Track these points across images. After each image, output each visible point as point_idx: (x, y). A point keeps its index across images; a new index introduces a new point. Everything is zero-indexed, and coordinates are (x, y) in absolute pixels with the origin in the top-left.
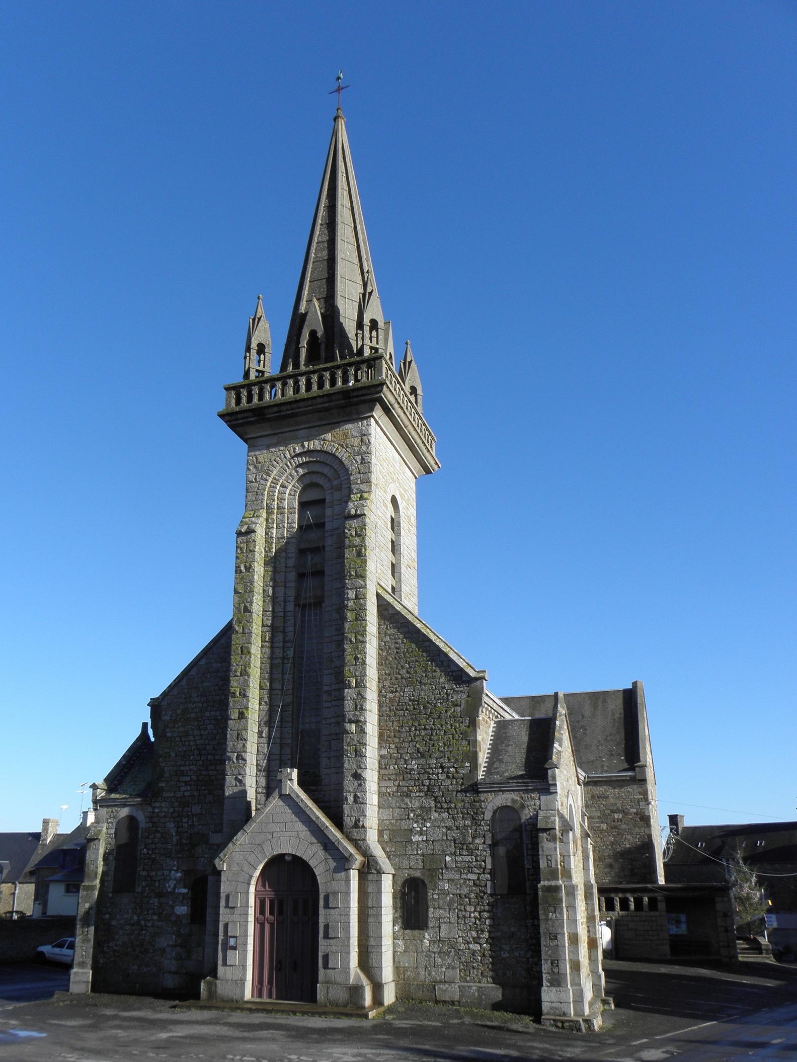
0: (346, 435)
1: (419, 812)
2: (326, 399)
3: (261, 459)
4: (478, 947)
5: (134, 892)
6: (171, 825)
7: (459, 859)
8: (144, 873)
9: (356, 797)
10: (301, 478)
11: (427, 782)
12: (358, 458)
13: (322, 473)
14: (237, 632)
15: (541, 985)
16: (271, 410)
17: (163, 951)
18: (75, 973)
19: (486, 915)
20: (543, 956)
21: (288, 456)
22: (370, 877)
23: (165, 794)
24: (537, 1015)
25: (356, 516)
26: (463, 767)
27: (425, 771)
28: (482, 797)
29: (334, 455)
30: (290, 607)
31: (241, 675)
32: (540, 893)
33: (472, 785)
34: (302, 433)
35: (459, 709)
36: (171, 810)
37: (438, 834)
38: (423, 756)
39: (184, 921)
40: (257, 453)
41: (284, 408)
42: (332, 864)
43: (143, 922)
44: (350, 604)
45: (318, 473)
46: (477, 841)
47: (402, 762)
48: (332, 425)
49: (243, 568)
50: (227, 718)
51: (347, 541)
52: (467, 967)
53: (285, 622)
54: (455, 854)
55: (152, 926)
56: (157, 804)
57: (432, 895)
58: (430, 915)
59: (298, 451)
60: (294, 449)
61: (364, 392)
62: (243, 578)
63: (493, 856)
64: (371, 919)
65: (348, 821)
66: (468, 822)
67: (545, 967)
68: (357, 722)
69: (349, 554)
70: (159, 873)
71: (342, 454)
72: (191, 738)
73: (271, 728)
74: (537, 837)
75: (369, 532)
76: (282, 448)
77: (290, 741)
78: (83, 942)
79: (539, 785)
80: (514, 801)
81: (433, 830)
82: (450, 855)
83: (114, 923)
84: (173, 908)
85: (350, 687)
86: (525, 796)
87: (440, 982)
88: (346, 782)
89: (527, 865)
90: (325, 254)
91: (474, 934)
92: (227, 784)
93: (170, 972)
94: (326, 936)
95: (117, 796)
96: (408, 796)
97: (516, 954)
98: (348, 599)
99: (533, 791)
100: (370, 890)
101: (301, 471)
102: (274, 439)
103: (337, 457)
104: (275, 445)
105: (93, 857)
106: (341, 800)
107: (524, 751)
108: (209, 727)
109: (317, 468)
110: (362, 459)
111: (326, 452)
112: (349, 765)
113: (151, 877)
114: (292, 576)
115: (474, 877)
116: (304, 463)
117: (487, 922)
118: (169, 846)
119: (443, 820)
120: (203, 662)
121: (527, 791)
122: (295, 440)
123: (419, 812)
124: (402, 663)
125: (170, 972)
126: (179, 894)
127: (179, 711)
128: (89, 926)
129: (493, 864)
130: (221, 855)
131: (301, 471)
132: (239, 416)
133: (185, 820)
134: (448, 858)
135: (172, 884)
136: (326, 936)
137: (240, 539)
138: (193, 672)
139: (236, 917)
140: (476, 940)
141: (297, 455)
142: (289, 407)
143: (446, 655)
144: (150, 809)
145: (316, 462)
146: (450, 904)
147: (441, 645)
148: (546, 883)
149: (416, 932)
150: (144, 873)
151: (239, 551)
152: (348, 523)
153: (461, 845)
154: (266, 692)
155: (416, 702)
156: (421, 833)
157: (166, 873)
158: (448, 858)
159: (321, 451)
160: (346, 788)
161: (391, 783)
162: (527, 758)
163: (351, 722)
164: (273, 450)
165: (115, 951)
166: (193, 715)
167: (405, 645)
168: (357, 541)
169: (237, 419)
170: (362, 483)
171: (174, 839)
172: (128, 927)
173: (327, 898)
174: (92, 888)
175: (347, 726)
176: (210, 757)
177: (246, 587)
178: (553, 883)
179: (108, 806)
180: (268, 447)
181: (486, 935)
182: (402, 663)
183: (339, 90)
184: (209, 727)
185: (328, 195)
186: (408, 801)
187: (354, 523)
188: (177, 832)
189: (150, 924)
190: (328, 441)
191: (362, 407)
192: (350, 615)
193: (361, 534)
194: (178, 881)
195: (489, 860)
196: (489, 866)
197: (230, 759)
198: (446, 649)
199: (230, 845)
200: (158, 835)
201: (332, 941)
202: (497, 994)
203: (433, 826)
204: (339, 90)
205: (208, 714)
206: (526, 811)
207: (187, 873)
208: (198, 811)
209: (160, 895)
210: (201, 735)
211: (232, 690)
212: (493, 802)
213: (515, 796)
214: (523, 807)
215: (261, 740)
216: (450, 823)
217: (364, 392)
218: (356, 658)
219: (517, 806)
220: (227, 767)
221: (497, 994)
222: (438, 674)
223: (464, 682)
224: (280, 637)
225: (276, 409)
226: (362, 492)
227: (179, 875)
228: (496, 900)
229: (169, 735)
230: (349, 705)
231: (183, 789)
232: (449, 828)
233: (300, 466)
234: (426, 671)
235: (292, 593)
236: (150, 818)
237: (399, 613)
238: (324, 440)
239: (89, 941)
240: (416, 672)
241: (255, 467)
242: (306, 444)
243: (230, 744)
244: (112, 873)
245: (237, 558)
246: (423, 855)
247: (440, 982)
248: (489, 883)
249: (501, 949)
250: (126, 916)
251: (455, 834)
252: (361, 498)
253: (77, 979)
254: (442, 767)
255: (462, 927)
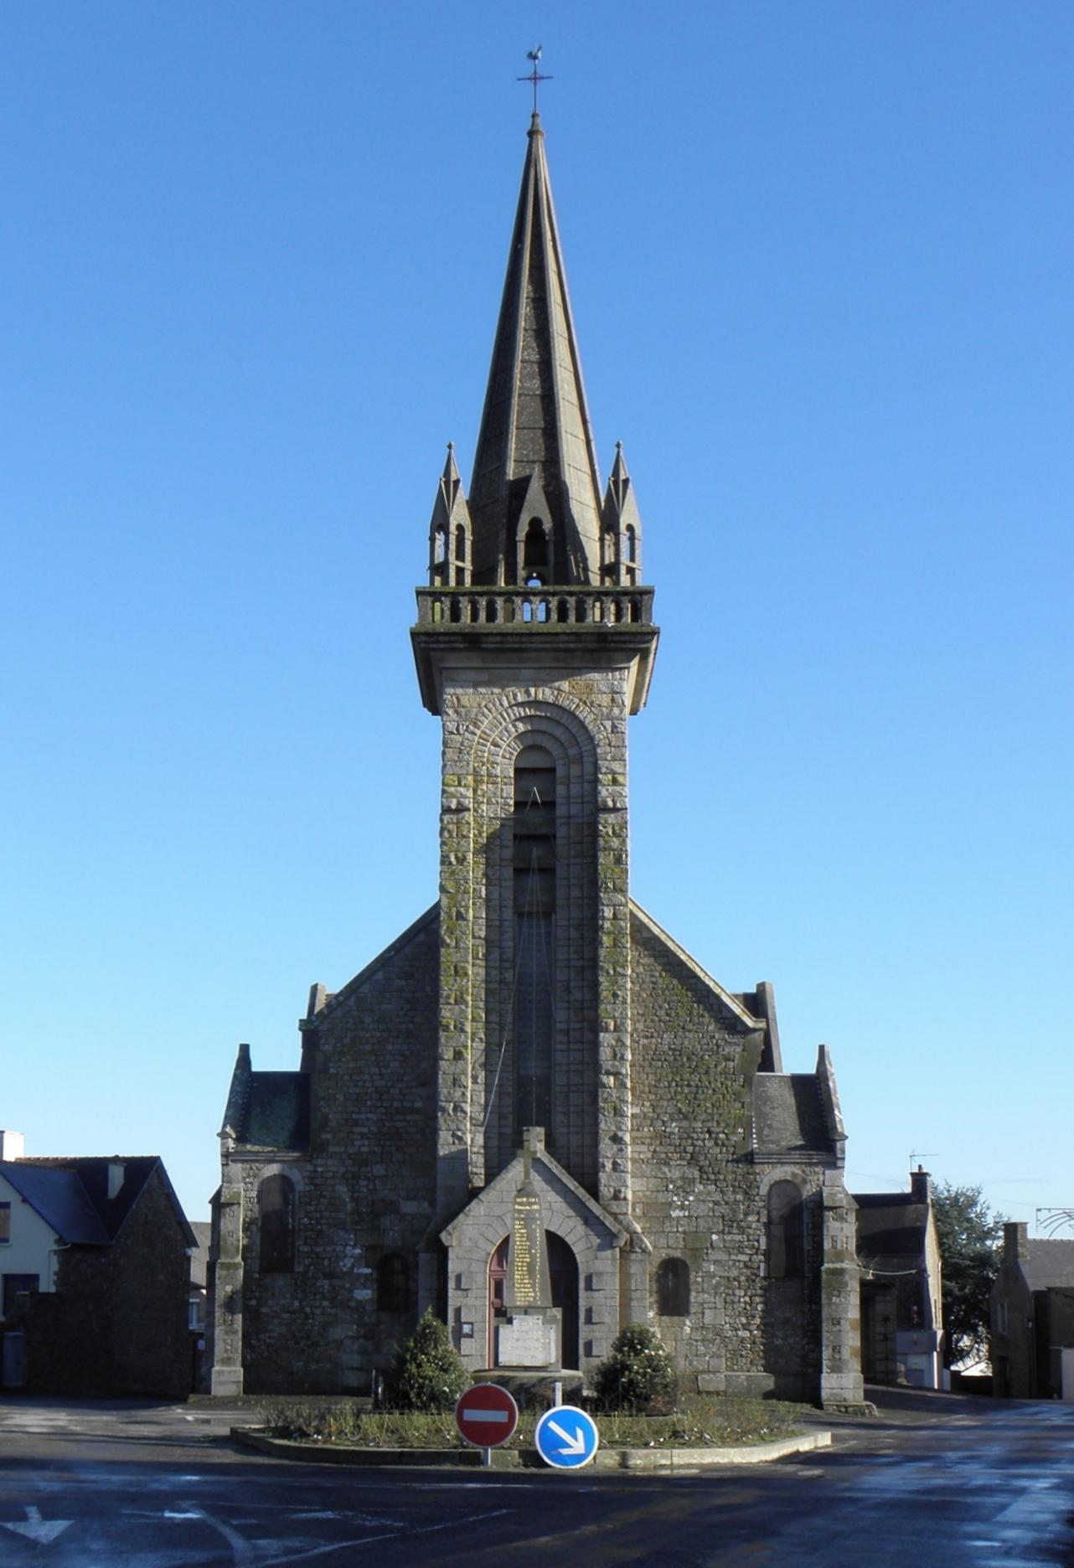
0: (590, 688)
1: (679, 1183)
2: (572, 638)
3: (465, 701)
4: (748, 1334)
5: (292, 1271)
6: (343, 1190)
7: (729, 1238)
8: (306, 1249)
9: (615, 1164)
10: (520, 737)
11: (690, 1149)
12: (608, 724)
13: (551, 735)
14: (448, 946)
15: (820, 1372)
16: (491, 639)
17: (339, 1344)
18: (219, 1372)
19: (758, 1299)
20: (825, 1342)
21: (506, 704)
22: (633, 1256)
23: (332, 1149)
24: (818, 1404)
25: (615, 810)
26: (734, 1133)
27: (687, 1135)
28: (758, 1169)
29: (572, 714)
30: (508, 914)
31: (456, 1003)
32: (824, 1276)
33: (746, 1155)
34: (526, 674)
35: (731, 1064)
36: (342, 1169)
37: (703, 1209)
38: (686, 1118)
39: (368, 1308)
40: (459, 691)
41: (510, 639)
42: (596, 1241)
43: (308, 1310)
44: (607, 925)
45: (545, 733)
46: (750, 1218)
47: (660, 1123)
48: (571, 671)
49: (453, 859)
50: (436, 1058)
51: (601, 842)
52: (735, 1355)
53: (501, 934)
54: (723, 1232)
55: (323, 1314)
56: (320, 1162)
57: (695, 1278)
58: (692, 1300)
59: (520, 699)
60: (515, 696)
61: (627, 638)
62: (453, 873)
63: (768, 1235)
64: (634, 1303)
65: (606, 1191)
66: (739, 1197)
67: (826, 1353)
68: (616, 1074)
69: (605, 860)
70: (328, 1249)
71: (584, 714)
72: (367, 1077)
73: (489, 1073)
74: (821, 1216)
75: (630, 831)
76: (497, 691)
77: (510, 1090)
78: (227, 1333)
79: (824, 1156)
80: (794, 1175)
81: (696, 1204)
82: (717, 1233)
83: (264, 1310)
84: (351, 1292)
85: (607, 1030)
86: (807, 1169)
87: (703, 1372)
88: (602, 1146)
89: (807, 1247)
90: (535, 384)
91: (744, 1320)
92: (441, 1141)
93: (352, 1369)
94: (589, 1321)
95: (256, 1148)
96: (666, 1164)
97: (791, 1341)
98: (604, 918)
99: (816, 1164)
100: (633, 1270)
101: (521, 727)
102: (485, 676)
103: (577, 718)
104: (488, 684)
105: (231, 1227)
106: (596, 1167)
107: (795, 1116)
108: (392, 1064)
109: (544, 726)
110: (614, 726)
111: (560, 707)
112: (606, 1125)
113: (317, 1254)
114: (509, 872)
115: (746, 1258)
116: (527, 717)
117: (760, 1307)
118: (342, 1216)
119: (709, 1194)
120: (379, 976)
121: (810, 1164)
122: (516, 681)
123: (679, 1183)
124: (660, 1001)
125: (352, 1369)
126: (360, 1275)
127: (347, 1041)
128: (233, 1313)
129: (768, 1244)
130: (449, 1228)
131: (521, 727)
132: (441, 638)
133: (363, 1183)
134: (714, 1237)
135: (349, 1262)
136: (589, 1321)
137: (447, 818)
138: (366, 988)
139: (470, 1301)
140: (745, 1327)
141: (522, 704)
142: (517, 639)
143: (717, 997)
144: (309, 1167)
145: (545, 717)
146: (717, 1287)
147: (711, 984)
148: (831, 1266)
149: (676, 1318)
150: (306, 1249)
151: (446, 834)
152: (602, 817)
153: (730, 1223)
154: (480, 1025)
155: (678, 1052)
156: (682, 1208)
157: (339, 1248)
158: (714, 1237)
159: (553, 705)
160: (603, 1153)
161: (644, 1148)
162: (801, 1125)
163: (608, 1073)
164: (482, 690)
165: (269, 1345)
166: (368, 1047)
167: (663, 980)
168: (615, 843)
169: (437, 642)
170: (614, 759)
171: (349, 1206)
172: (286, 1316)
173: (589, 1279)
174: (235, 1266)
175: (604, 1079)
176: (396, 1104)
177: (457, 885)
178: (838, 1266)
179: (243, 1162)
180: (475, 686)
181: (758, 1321)
182: (660, 1001)
183: (535, 78)
184: (392, 1064)
185: (531, 276)
186: (666, 1169)
187: (611, 818)
188: (352, 1198)
189: (318, 1311)
190: (564, 691)
191: (617, 655)
192: (606, 940)
193: (620, 832)
194: (357, 1259)
195: (763, 1240)
196: (763, 1247)
197: (444, 1110)
198: (717, 991)
199: (461, 1216)
200: (325, 1201)
201: (595, 1327)
202: (769, 1382)
203: (697, 1200)
204: (535, 78)
205: (390, 1047)
206: (808, 1187)
207: (368, 1249)
208: (383, 1172)
209: (330, 1276)
210: (381, 1075)
211: (444, 1021)
212: (770, 1175)
213: (797, 1170)
214: (805, 1181)
215: (476, 1087)
216: (717, 1197)
217: (627, 638)
218: (615, 995)
219: (798, 1181)
220: (441, 1121)
221: (769, 1382)
222: (706, 1020)
223: (739, 1033)
224: (496, 954)
225: (498, 639)
226: (614, 773)
227: (358, 1251)
228: (770, 1284)
229: (332, 1071)
230: (605, 1053)
231: (357, 1143)
232: (716, 1203)
233: (520, 719)
234: (691, 1014)
235: (509, 895)
236: (312, 1178)
237: (656, 938)
238: (559, 689)
239: (235, 1332)
240: (677, 1015)
241: (456, 712)
242: (532, 690)
243: (443, 1092)
244: (257, 1247)
245: (443, 843)
246: (684, 1232)
247: (703, 1372)
248: (762, 1266)
249: (774, 1336)
250: (282, 1302)
251: (724, 1209)
252: (615, 782)
253: (222, 1378)
254: (709, 1132)
255: (729, 1312)
